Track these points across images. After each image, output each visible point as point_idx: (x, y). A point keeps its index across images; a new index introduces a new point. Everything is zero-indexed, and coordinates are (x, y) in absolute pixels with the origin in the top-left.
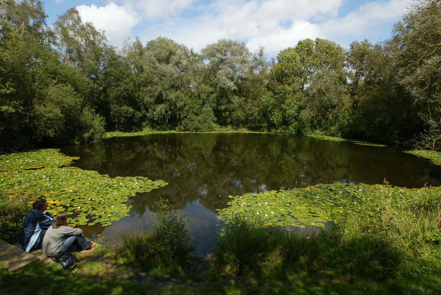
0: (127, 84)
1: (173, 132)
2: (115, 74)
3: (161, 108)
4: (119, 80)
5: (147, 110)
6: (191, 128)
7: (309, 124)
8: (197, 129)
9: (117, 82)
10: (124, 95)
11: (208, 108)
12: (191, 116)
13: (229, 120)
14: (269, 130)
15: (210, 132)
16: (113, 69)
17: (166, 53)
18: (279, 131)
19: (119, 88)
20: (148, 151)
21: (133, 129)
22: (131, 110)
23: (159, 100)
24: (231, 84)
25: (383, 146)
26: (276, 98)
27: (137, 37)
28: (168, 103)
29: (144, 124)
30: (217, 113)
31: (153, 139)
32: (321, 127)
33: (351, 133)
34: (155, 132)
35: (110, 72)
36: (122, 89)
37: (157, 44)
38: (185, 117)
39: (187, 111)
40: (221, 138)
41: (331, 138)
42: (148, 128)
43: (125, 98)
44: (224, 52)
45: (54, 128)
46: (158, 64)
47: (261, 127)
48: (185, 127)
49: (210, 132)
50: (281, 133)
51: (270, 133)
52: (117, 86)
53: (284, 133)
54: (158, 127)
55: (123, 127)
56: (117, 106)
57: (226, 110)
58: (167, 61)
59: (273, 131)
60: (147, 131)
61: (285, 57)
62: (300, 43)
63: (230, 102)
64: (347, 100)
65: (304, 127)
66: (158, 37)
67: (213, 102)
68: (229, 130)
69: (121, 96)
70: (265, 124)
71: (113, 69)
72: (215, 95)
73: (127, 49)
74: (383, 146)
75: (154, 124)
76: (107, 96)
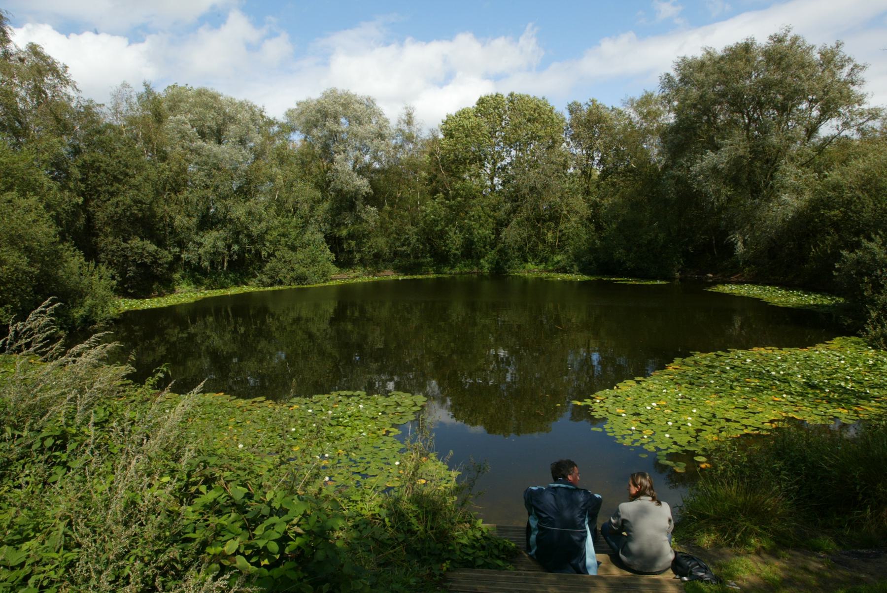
0: (137, 188)
1: (245, 289)
2: (108, 165)
3: (211, 239)
4: (119, 181)
5: (181, 245)
6: (285, 277)
7: (517, 254)
8: (301, 279)
9: (112, 185)
10: (132, 214)
11: (315, 235)
12: (283, 252)
13: (358, 256)
14: (438, 272)
15: (327, 284)
16: (99, 154)
17: (217, 121)
18: (457, 270)
19: (121, 198)
20: (191, 337)
21: (153, 291)
22: (152, 248)
23: (207, 222)
24: (362, 184)
25: (664, 283)
26: (450, 207)
27: (148, 83)
28: (230, 226)
29: (177, 276)
30: (334, 242)
31: (199, 309)
32: (535, 256)
33: (600, 263)
34: (204, 293)
35: (94, 162)
36: (128, 201)
37: (191, 100)
38: (270, 255)
39: (275, 243)
40: (345, 293)
41: (560, 277)
42: (184, 286)
43: (135, 221)
44: (327, 120)
45: (12, 303)
46: (200, 143)
47: (420, 265)
48: (272, 278)
49: (327, 284)
50: (461, 273)
51: (440, 275)
52: (112, 194)
53: (469, 273)
54: (206, 281)
55: (131, 288)
56: (117, 240)
57: (351, 236)
58: (218, 136)
59: (447, 272)
60: (185, 294)
61: (454, 128)
62: (481, 102)
63: (358, 219)
64: (580, 204)
65: (508, 260)
66: (171, 84)
67: (325, 220)
68: (359, 277)
69: (125, 216)
70: (429, 259)
71: (99, 154)
72: (326, 205)
73: (124, 107)
74: (664, 283)
75: (197, 274)
76: (90, 219)
